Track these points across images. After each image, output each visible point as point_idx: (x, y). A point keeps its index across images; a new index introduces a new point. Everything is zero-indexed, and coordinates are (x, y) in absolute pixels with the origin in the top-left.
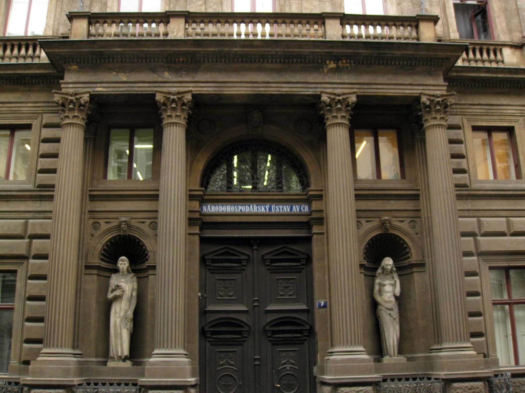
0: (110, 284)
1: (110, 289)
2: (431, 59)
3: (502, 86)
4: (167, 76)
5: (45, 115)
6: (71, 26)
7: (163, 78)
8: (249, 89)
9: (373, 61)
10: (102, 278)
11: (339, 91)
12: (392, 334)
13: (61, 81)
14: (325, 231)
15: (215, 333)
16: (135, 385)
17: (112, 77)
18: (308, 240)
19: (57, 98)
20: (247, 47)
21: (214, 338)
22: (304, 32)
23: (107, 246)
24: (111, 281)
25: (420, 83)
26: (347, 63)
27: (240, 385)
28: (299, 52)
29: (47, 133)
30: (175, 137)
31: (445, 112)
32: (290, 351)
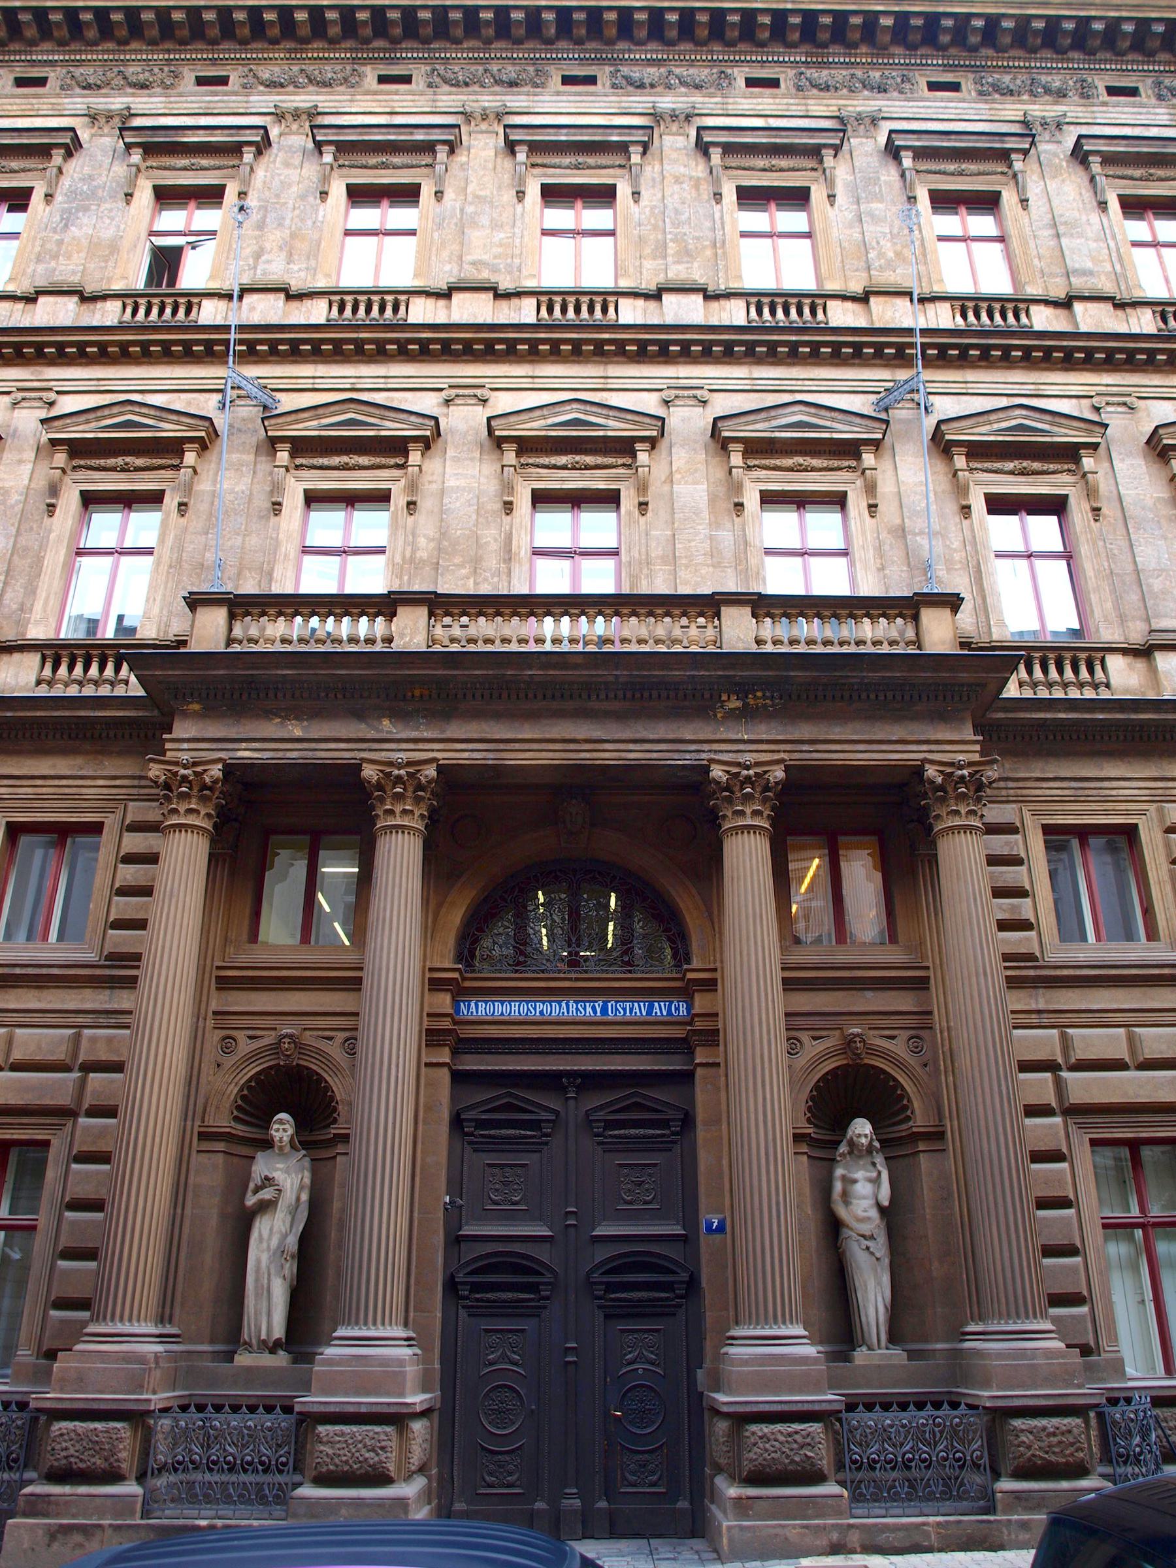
1: (252, 1186)
4: (387, 726)
5: (131, 804)
6: (193, 621)
7: (378, 730)
8: (557, 755)
10: (235, 1160)
11: (748, 758)
12: (873, 1295)
14: (720, 1060)
15: (481, 1286)
16: (288, 1410)
18: (687, 1077)
19: (155, 771)
20: (555, 667)
21: (477, 1300)
22: (677, 632)
23: (250, 1088)
25: (923, 738)
26: (764, 697)
27: (532, 1411)
28: (663, 676)
29: (134, 842)
30: (401, 856)
31: (978, 800)
32: (510, 1331)
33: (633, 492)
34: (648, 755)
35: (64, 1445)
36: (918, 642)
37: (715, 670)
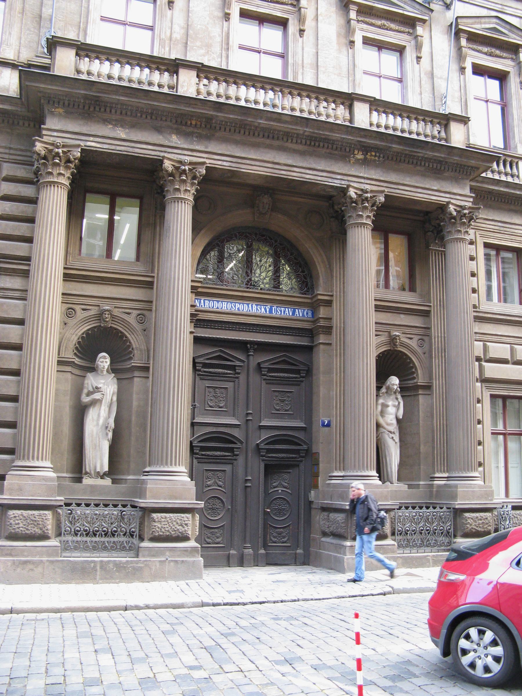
0: (86, 385)
1: (85, 391)
2: (461, 165)
3: (516, 203)
4: (175, 140)
7: (169, 141)
9: (403, 159)
13: (42, 126)
17: (107, 130)
18: (309, 349)
20: (274, 120)
24: (86, 382)
25: (448, 190)
26: (375, 156)
27: (229, 509)
30: (181, 216)
33: (296, 22)
34: (316, 178)
35: (17, 522)
36: (351, 121)
37: (357, 137)
